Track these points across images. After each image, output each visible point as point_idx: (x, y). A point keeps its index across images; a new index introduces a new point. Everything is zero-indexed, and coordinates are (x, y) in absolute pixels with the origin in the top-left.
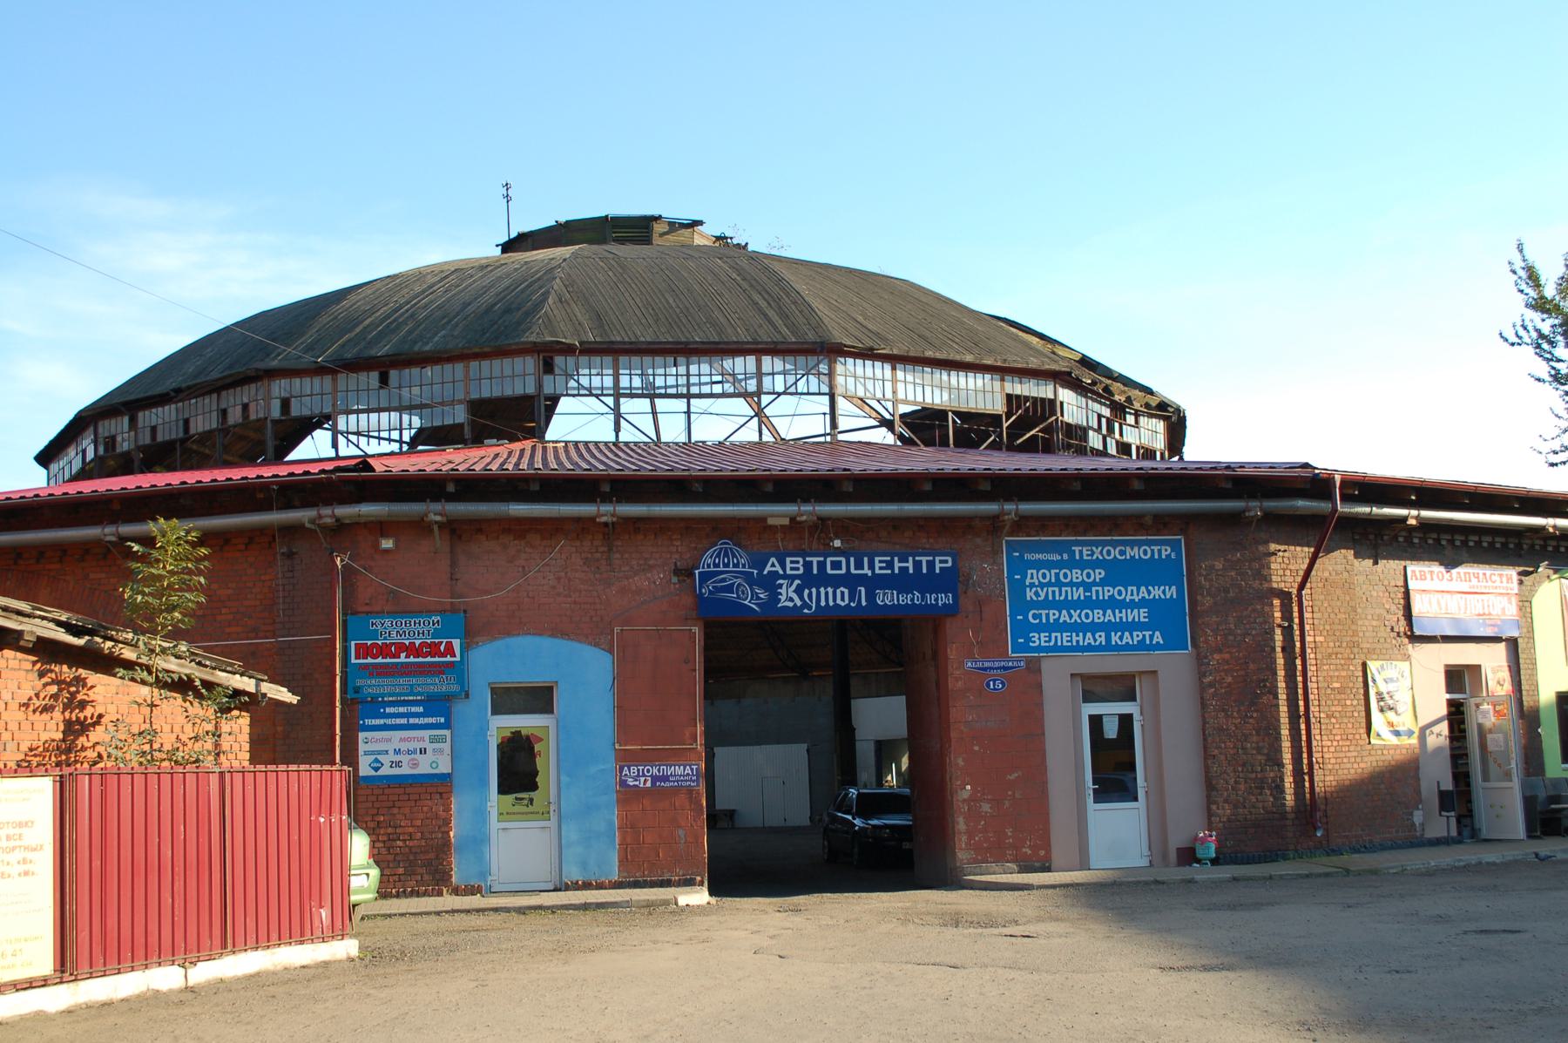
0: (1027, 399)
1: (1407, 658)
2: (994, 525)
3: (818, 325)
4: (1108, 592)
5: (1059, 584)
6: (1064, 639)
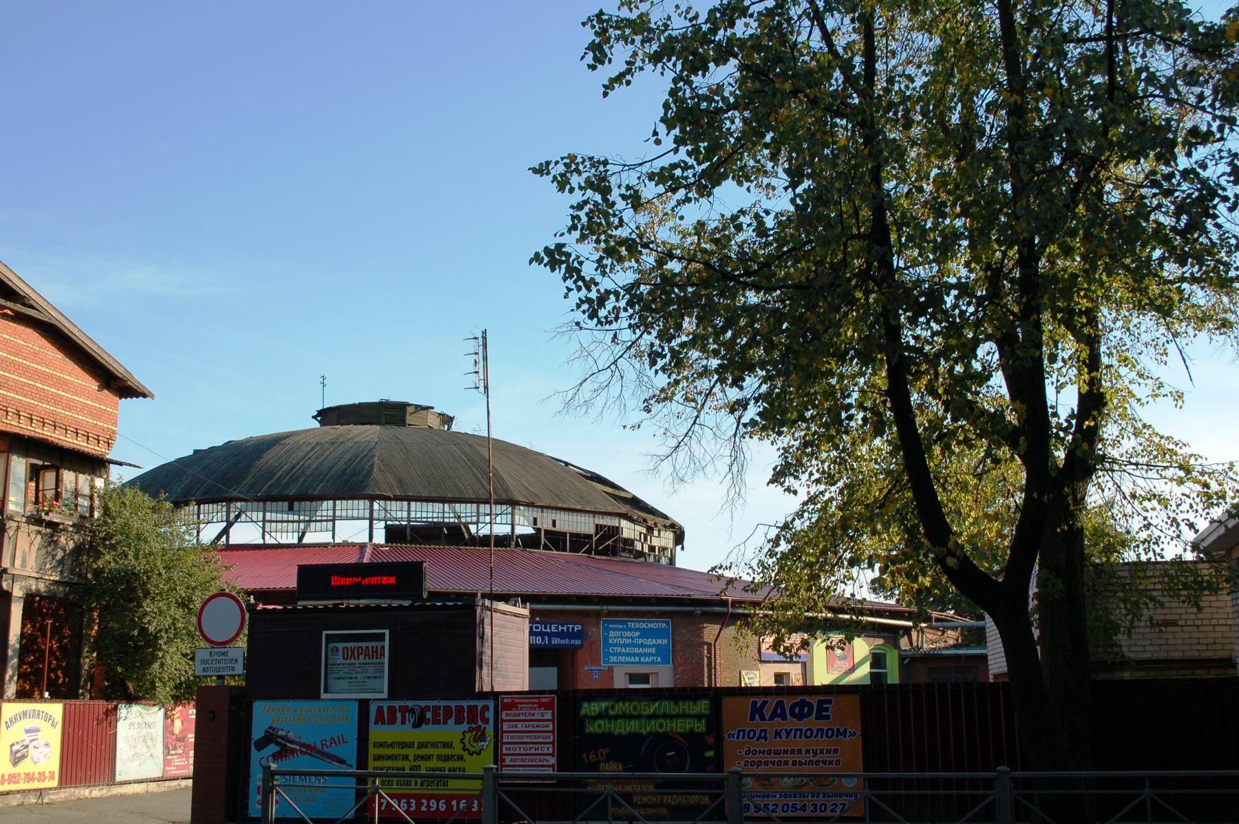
0: (605, 526)
1: (758, 669)
2: (598, 614)
3: (507, 490)
4: (640, 641)
5: (622, 637)
6: (623, 659)
